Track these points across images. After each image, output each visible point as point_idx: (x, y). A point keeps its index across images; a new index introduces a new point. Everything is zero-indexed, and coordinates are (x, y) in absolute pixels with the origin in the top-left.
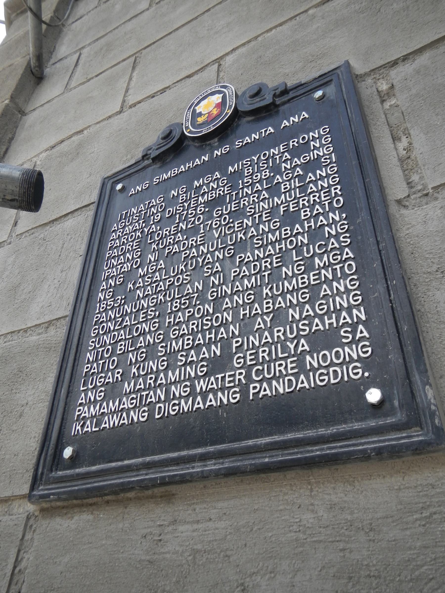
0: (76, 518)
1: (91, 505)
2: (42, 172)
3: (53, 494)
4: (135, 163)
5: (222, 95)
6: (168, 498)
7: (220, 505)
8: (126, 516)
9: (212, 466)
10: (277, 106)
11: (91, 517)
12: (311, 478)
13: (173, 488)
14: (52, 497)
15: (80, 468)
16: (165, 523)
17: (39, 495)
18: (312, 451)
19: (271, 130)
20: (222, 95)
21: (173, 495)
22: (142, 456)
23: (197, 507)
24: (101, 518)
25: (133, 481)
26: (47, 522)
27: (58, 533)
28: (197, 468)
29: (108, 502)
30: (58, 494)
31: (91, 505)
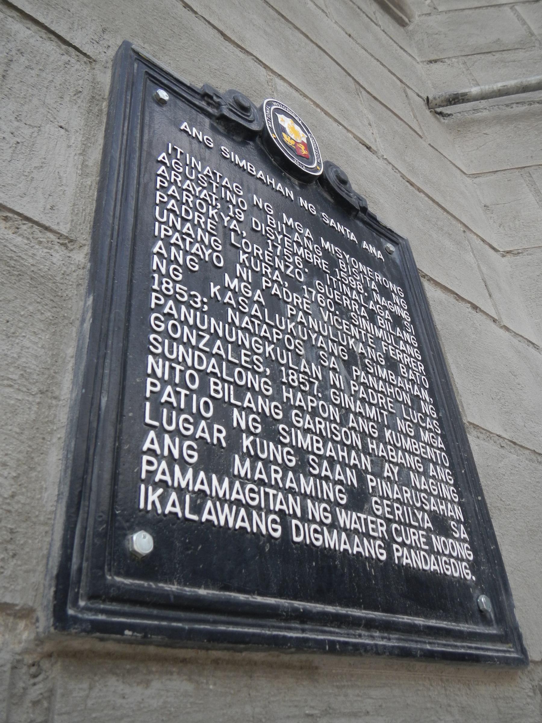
0: (156, 685)
1: (184, 661)
2: (328, 159)
3: (131, 627)
4: (189, 88)
5: (278, 115)
6: (310, 671)
7: (374, 693)
8: (253, 693)
9: (378, 640)
10: (356, 217)
11: (188, 687)
12: (443, 674)
13: (317, 659)
14: (127, 632)
15: (165, 582)
16: (317, 712)
17: (92, 622)
18: (456, 647)
19: (365, 245)
20: (278, 115)
21: (317, 668)
22: (280, 595)
23: (350, 692)
24: (211, 690)
25: (291, 638)
26: (85, 686)
27: (119, 713)
28: (364, 638)
29: (216, 662)
30: (143, 629)
31: (184, 661)
